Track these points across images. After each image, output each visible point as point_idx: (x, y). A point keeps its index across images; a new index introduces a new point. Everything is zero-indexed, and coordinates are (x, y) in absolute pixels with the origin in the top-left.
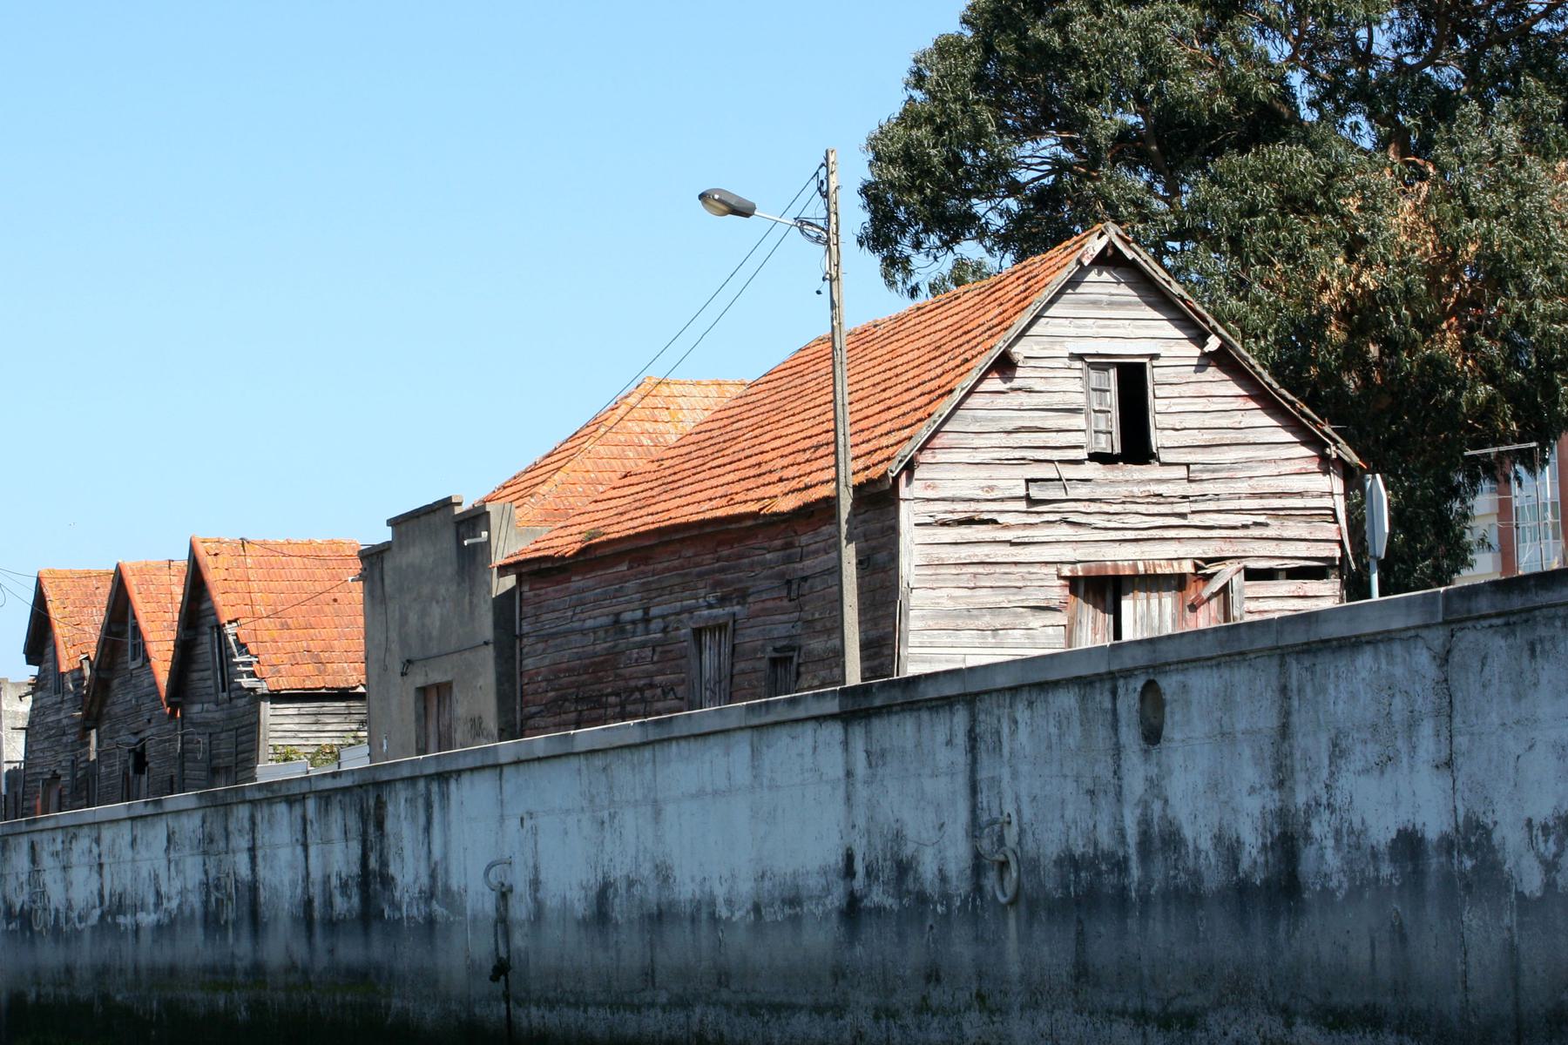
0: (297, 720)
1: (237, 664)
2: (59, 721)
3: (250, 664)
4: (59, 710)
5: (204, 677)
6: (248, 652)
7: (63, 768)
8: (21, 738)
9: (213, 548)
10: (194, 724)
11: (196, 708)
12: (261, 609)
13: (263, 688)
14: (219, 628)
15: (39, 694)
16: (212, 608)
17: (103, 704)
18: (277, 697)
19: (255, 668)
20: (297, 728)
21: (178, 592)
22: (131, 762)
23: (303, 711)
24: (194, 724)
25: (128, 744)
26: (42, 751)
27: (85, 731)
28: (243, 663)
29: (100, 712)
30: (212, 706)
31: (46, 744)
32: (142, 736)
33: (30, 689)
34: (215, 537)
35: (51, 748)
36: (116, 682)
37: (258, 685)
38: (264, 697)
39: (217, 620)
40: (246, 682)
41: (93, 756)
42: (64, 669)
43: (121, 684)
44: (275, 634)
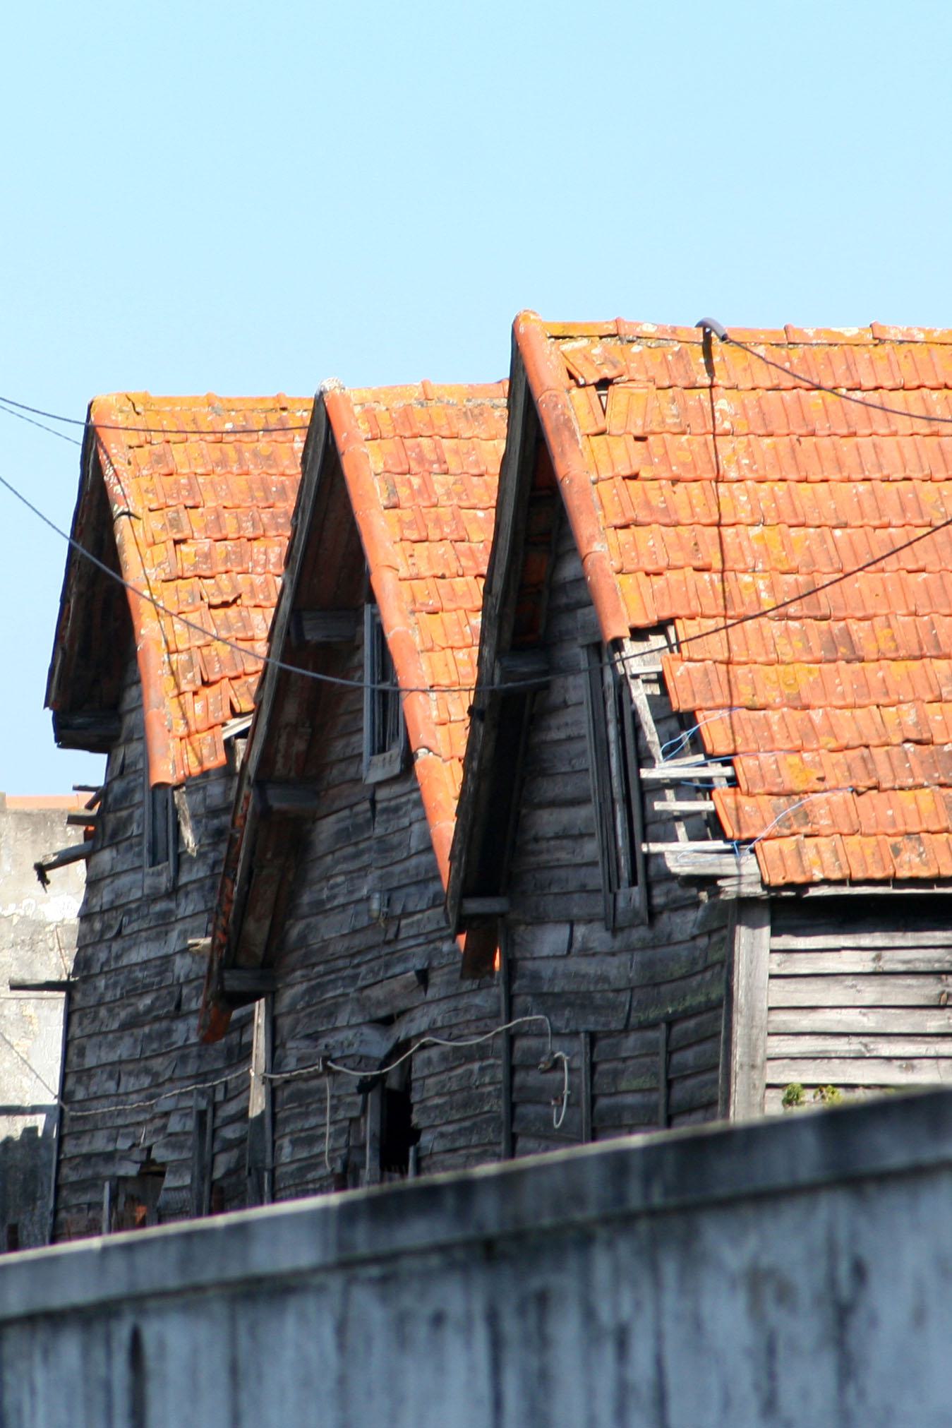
0: (870, 992)
1: (659, 787)
2: (167, 960)
3: (705, 788)
4: (165, 922)
5: (564, 828)
6: (697, 744)
7: (174, 1141)
8: (50, 1014)
9: (595, 359)
10: (549, 1001)
11: (552, 939)
12: (755, 587)
13: (745, 875)
14: (604, 650)
15: (106, 858)
16: (581, 580)
17: (284, 909)
18: (793, 910)
19: (722, 802)
20: (870, 1022)
21: (480, 529)
22: (370, 1126)
23: (891, 961)
24: (549, 1001)
25: (362, 1061)
26: (115, 1070)
27: (225, 1008)
28: (677, 785)
29: (277, 932)
30: (593, 935)
31: (124, 1049)
32: (401, 1031)
33: (74, 837)
34: (603, 318)
35: (139, 1064)
36: (326, 829)
37: (727, 865)
38: (745, 908)
39: (596, 626)
40: (682, 855)
41: (257, 1104)
42: (165, 770)
43: (344, 836)
44: (805, 676)
